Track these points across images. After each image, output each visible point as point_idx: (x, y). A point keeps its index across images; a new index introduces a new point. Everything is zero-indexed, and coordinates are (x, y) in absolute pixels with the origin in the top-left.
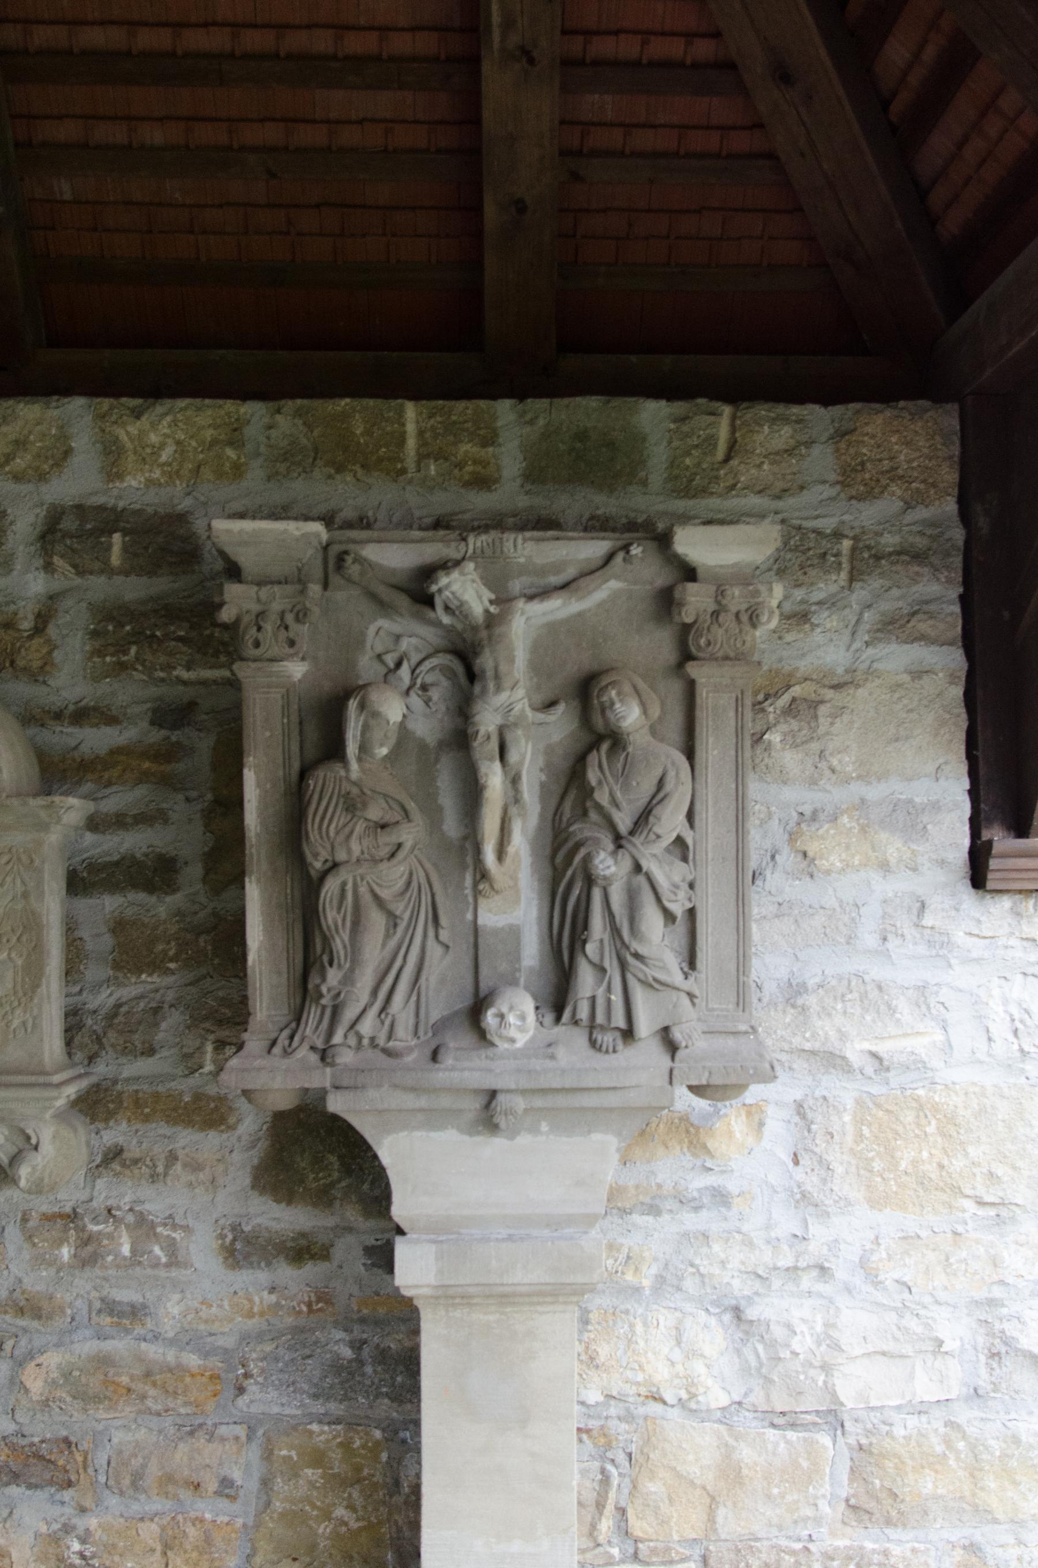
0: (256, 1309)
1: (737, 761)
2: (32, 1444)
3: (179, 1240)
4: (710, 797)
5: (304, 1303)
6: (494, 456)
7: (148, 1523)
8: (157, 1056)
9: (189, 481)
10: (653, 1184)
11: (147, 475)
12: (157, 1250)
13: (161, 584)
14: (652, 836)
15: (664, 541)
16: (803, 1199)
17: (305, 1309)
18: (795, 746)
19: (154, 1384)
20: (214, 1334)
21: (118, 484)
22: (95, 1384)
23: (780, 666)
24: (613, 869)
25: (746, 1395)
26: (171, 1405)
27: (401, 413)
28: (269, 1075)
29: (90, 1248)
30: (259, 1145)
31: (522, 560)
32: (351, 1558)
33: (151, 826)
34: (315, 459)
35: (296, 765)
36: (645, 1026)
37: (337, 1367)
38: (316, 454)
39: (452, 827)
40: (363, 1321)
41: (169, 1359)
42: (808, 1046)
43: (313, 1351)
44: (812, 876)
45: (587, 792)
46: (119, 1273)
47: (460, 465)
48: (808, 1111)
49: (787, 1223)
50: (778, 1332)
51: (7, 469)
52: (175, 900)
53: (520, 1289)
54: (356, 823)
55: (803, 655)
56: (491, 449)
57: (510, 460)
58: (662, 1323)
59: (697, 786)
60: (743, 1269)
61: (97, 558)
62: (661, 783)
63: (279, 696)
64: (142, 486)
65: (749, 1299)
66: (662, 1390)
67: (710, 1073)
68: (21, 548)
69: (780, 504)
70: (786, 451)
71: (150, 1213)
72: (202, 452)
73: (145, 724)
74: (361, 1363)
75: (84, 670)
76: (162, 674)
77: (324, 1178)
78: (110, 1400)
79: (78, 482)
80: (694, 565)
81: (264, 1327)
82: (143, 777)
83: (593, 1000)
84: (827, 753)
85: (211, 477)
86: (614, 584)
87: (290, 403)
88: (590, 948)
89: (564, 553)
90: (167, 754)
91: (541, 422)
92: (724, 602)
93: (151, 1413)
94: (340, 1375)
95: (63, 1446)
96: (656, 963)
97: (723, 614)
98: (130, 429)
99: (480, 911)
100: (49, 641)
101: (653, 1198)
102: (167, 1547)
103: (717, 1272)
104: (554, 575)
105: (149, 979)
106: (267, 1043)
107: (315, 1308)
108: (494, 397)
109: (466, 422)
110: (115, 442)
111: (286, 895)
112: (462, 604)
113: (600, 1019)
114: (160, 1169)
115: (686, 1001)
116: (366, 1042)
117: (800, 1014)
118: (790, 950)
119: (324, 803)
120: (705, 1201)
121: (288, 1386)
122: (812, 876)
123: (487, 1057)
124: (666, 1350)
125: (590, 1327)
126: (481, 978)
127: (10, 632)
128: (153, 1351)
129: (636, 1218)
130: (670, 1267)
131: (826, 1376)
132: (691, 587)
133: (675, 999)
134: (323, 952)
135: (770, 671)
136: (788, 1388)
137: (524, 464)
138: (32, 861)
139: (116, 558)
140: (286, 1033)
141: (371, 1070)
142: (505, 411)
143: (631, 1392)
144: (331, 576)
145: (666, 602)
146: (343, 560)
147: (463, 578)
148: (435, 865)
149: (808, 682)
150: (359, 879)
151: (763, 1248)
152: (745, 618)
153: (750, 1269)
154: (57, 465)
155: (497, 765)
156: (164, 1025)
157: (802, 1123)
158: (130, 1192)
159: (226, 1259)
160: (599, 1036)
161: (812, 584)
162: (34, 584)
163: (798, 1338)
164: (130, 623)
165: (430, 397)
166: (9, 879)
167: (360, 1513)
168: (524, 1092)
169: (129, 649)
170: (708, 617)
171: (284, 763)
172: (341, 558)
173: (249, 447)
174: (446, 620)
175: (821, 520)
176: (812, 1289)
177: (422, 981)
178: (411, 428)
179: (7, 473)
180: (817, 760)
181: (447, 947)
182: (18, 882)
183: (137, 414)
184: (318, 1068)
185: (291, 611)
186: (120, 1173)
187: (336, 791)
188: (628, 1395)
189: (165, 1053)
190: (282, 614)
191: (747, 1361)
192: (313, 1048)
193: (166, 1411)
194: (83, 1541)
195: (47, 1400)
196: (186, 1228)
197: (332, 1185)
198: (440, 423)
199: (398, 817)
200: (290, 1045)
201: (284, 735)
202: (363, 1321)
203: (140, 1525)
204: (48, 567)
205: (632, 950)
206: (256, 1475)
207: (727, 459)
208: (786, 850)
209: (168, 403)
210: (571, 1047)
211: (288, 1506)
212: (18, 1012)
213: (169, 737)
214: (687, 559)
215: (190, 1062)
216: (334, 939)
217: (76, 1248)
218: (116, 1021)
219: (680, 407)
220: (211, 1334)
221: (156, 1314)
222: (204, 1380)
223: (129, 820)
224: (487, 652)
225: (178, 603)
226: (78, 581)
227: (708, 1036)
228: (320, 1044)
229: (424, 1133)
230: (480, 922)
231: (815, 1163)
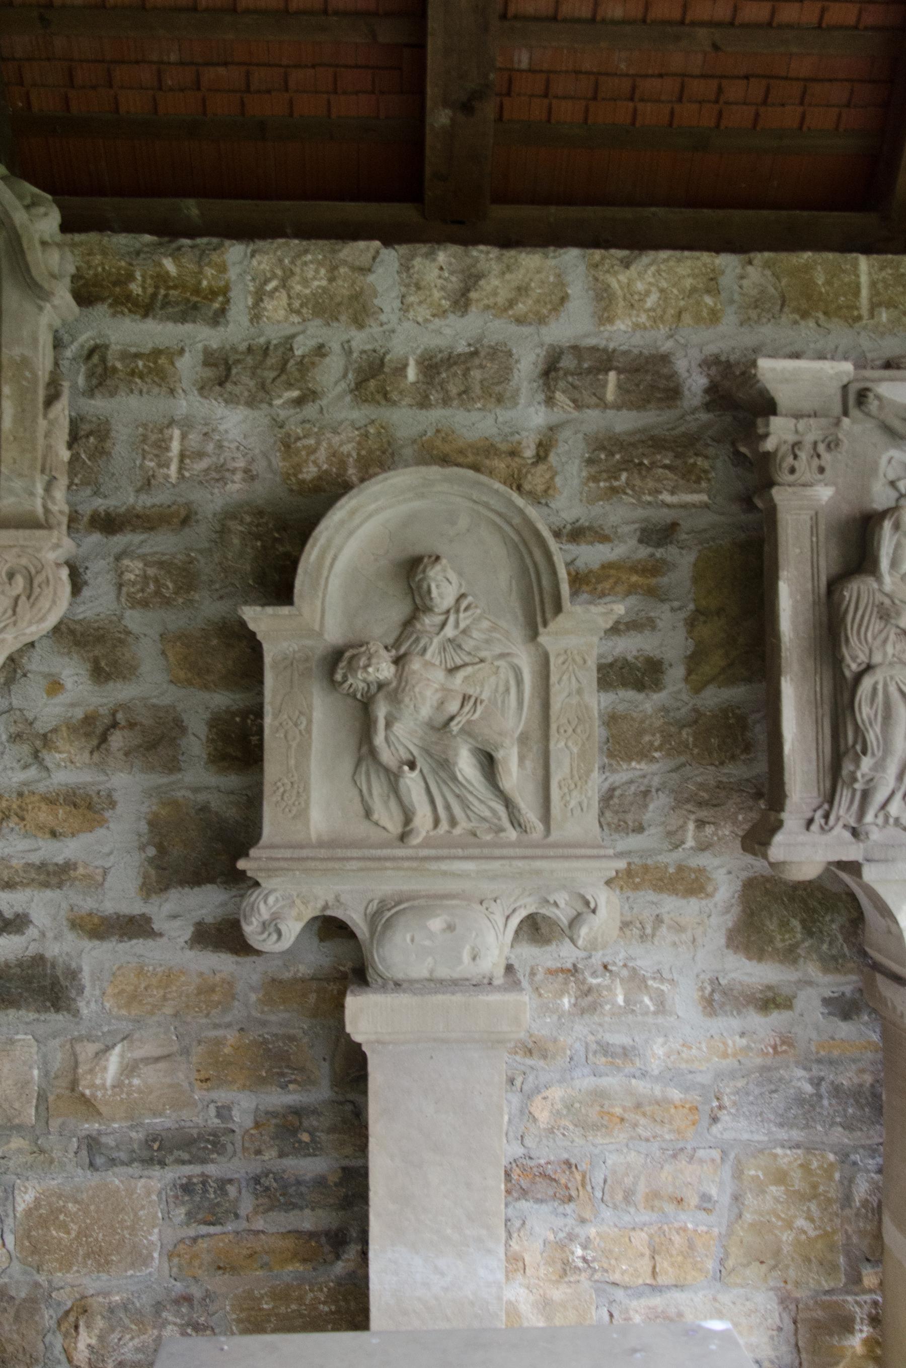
0: (730, 1051)
2: (539, 1166)
7: (639, 1232)
8: (646, 833)
12: (647, 1000)
17: (771, 1050)
19: (644, 1114)
22: (593, 1114)
27: (856, 266)
29: (590, 999)
32: (810, 1261)
37: (800, 1100)
40: (819, 1061)
51: (510, 313)
63: (808, 518)
68: (525, 384)
73: (633, 542)
74: (820, 1096)
75: (581, 493)
76: (649, 498)
78: (607, 1127)
79: (574, 325)
82: (632, 590)
85: (691, 322)
90: (654, 568)
95: (564, 1167)
100: (550, 468)
102: (654, 1253)
107: (779, 1049)
110: (606, 290)
114: (649, 931)
116: (891, 821)
127: (517, 459)
128: (641, 1086)
134: (855, 742)
138: (585, 662)
139: (610, 394)
140: (820, 813)
154: (555, 309)
156: (651, 807)
159: (705, 1008)
162: (531, 416)
164: (620, 452)
165: (879, 252)
166: (565, 677)
167: (818, 1223)
173: (724, 295)
178: (864, 279)
179: (510, 317)
182: (573, 680)
183: (626, 264)
185: (823, 441)
189: (652, 830)
190: (815, 444)
192: (845, 826)
193: (654, 1137)
194: (584, 1247)
195: (553, 1127)
200: (826, 823)
203: (632, 1234)
204: (550, 401)
206: (729, 1191)
209: (652, 254)
211: (756, 1217)
212: (575, 793)
215: (674, 839)
217: (577, 998)
218: (611, 802)
220: (691, 1072)
222: (686, 1111)
226: (575, 414)
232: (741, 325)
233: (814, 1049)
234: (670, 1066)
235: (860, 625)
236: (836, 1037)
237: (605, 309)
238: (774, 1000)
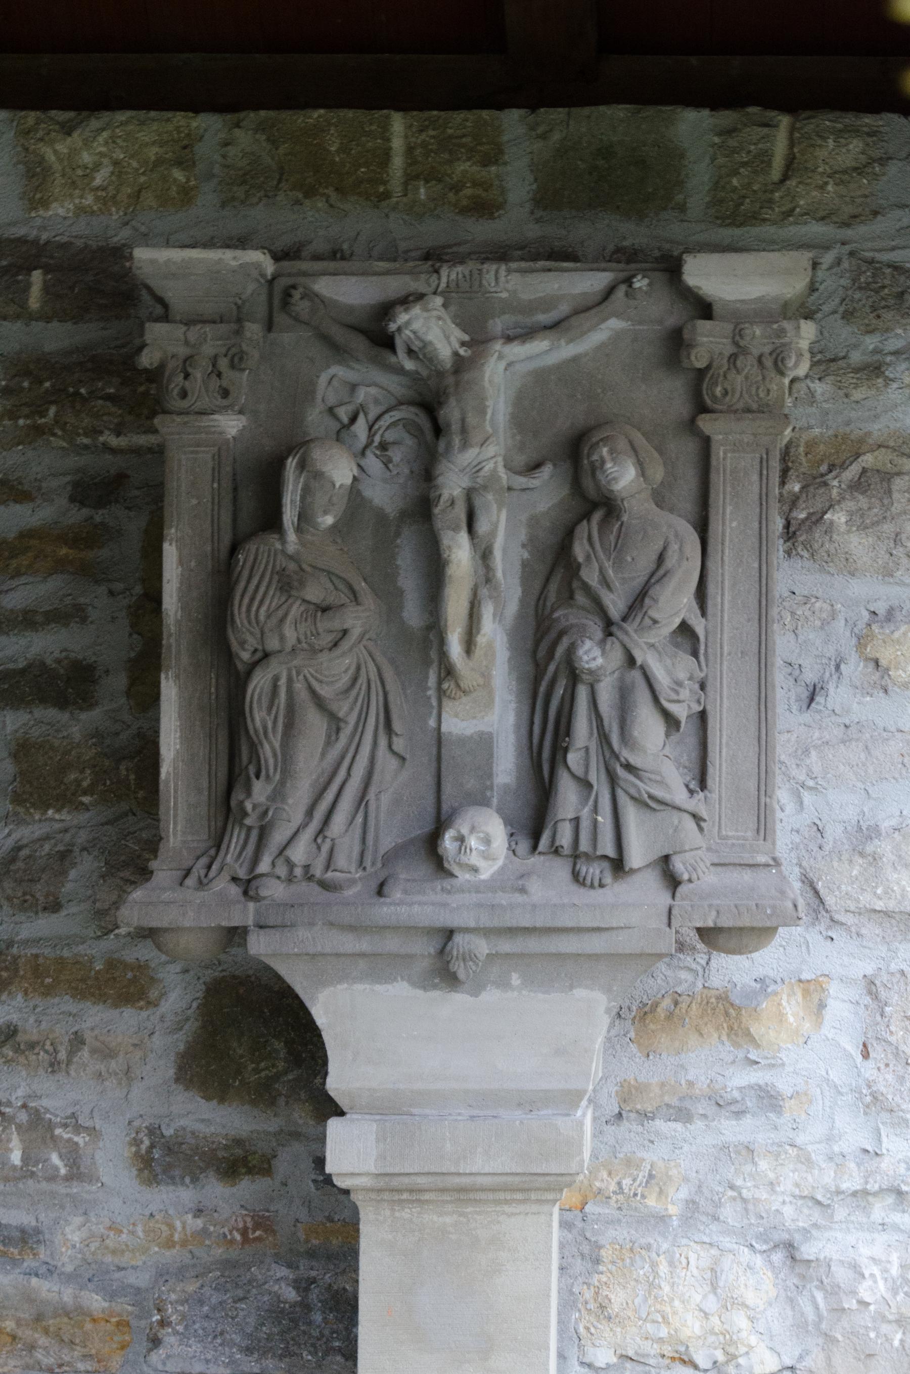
0: (176, 1237)
1: (760, 534)
3: (82, 1144)
4: (727, 577)
5: (238, 1230)
6: (498, 176)
8: (64, 913)
9: (127, 208)
10: (683, 1082)
11: (77, 201)
12: (55, 1159)
13: (88, 333)
14: (647, 621)
15: (671, 268)
16: (874, 1103)
17: (238, 1237)
18: (863, 527)
19: (46, 1331)
20: (124, 1269)
21: (41, 212)
23: (848, 430)
24: (600, 661)
25: (801, 1358)
26: (67, 1359)
27: (385, 127)
28: (180, 906)
30: (186, 1027)
31: (504, 295)
33: (66, 625)
34: (280, 181)
35: (227, 539)
36: (636, 856)
37: (277, 1312)
38: (282, 174)
39: (413, 614)
40: (312, 1254)
41: (65, 1299)
42: (879, 905)
43: (249, 1291)
44: (886, 691)
45: (573, 569)
46: (7, 1188)
47: (456, 188)
48: (881, 989)
49: (853, 1135)
50: (841, 1275)
52: (93, 717)
53: (480, 1180)
54: (291, 605)
55: (876, 417)
56: (493, 169)
57: (517, 180)
58: (693, 1262)
59: (710, 564)
60: (797, 1192)
61: (12, 300)
62: (661, 559)
63: (209, 456)
64: (70, 215)
65: (805, 1232)
66: (691, 1349)
67: (718, 912)
69: (849, 233)
70: (855, 169)
71: (47, 1111)
72: (143, 174)
73: (62, 501)
74: (306, 1307)
76: (86, 441)
77: (266, 1068)
80: (709, 299)
81: (187, 1259)
82: (60, 566)
83: (576, 821)
84: (904, 536)
85: (154, 204)
86: (614, 324)
87: (252, 114)
88: (573, 758)
89: (556, 286)
90: (86, 538)
91: (556, 136)
92: (742, 343)
93: (41, 1369)
94: (280, 1323)
96: (653, 776)
97: (741, 357)
98: (59, 147)
99: (444, 716)
101: (681, 1099)
103: (765, 1196)
104: (543, 313)
105: (57, 817)
106: (180, 874)
108: (500, 107)
109: (464, 136)
110: (40, 163)
111: (210, 694)
112: (426, 344)
113: (584, 845)
114: (62, 1055)
115: (690, 824)
116: (298, 871)
117: (870, 864)
118: (859, 785)
119: (255, 581)
120: (749, 1104)
121: (215, 1337)
122: (886, 691)
123: (442, 889)
124: (698, 1298)
125: (601, 1268)
126: (444, 797)
128: (46, 1289)
129: (660, 1124)
130: (705, 1190)
131: (904, 1333)
132: (704, 326)
133: (676, 822)
135: (836, 436)
136: (856, 1350)
137: (534, 187)
139: (35, 300)
140: (204, 861)
141: (302, 905)
142: (512, 122)
143: (652, 1352)
144: (275, 314)
145: (676, 344)
146: (290, 296)
147: (425, 314)
148: (392, 661)
149: (883, 450)
150: (294, 673)
151: (824, 1166)
152: (768, 363)
153: (806, 1193)
155: (463, 537)
156: (73, 874)
157: (873, 1005)
158: (23, 1084)
159: (140, 1170)
160: (583, 868)
161: (887, 330)
163: (868, 1283)
164: (50, 378)
168: (487, 932)
169: (47, 410)
170: (725, 360)
171: (213, 536)
172: (287, 294)
174: (409, 365)
175: (900, 252)
176: (887, 1220)
177: (371, 796)
178: (397, 144)
180: (892, 545)
181: (403, 759)
183: (67, 130)
184: (238, 902)
185: (225, 356)
186: (12, 1060)
187: (270, 567)
188: (648, 1355)
189: (73, 909)
190: (214, 360)
191: (802, 1314)
192: (234, 879)
196: (92, 1131)
197: (277, 1077)
198: (433, 137)
199: (344, 599)
200: (206, 876)
201: (213, 503)
202: (312, 1254)
205: (622, 759)
207: (785, 178)
208: (853, 658)
209: (106, 116)
210: (549, 888)
213: (92, 518)
214: (701, 292)
215: (104, 919)
216: (262, 745)
219: (727, 117)
220: (120, 1269)
221: (52, 1242)
223: (39, 618)
224: (452, 401)
225: (104, 352)
227: (720, 869)
228: (242, 874)
229: (368, 986)
230: (444, 728)
231: (890, 1056)
232: (223, 205)
233: (302, 1236)
234: (90, 1258)
235: (252, 599)
236: (336, 1218)
237: (37, 189)
238: (244, 1161)
